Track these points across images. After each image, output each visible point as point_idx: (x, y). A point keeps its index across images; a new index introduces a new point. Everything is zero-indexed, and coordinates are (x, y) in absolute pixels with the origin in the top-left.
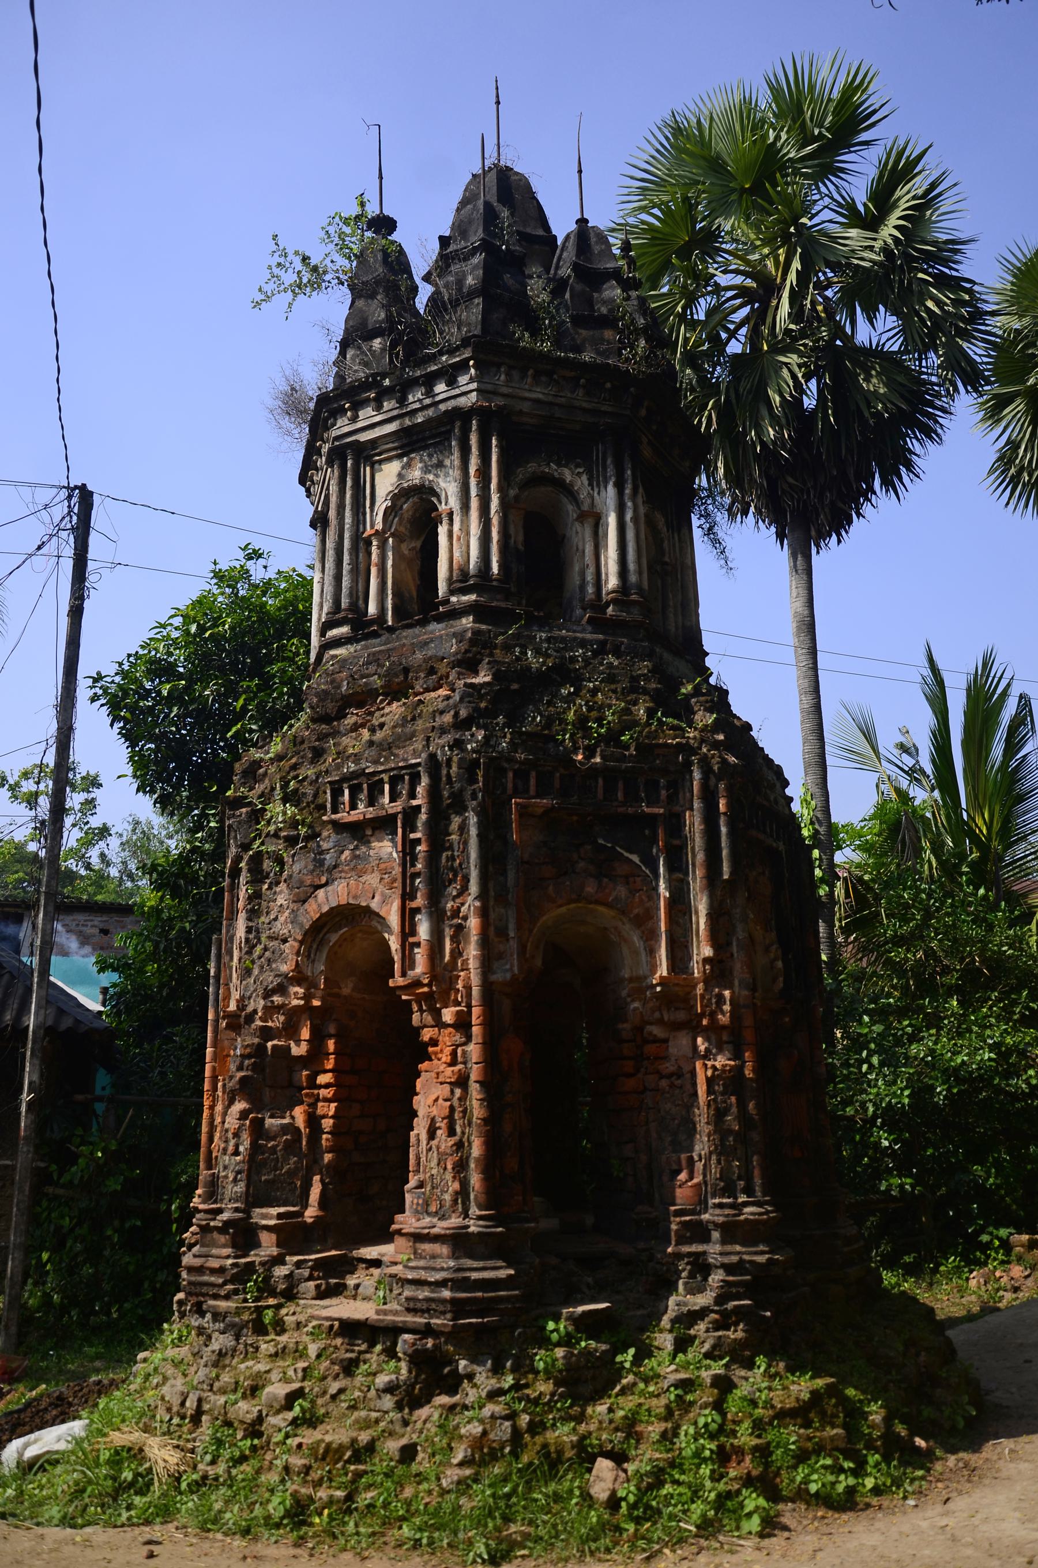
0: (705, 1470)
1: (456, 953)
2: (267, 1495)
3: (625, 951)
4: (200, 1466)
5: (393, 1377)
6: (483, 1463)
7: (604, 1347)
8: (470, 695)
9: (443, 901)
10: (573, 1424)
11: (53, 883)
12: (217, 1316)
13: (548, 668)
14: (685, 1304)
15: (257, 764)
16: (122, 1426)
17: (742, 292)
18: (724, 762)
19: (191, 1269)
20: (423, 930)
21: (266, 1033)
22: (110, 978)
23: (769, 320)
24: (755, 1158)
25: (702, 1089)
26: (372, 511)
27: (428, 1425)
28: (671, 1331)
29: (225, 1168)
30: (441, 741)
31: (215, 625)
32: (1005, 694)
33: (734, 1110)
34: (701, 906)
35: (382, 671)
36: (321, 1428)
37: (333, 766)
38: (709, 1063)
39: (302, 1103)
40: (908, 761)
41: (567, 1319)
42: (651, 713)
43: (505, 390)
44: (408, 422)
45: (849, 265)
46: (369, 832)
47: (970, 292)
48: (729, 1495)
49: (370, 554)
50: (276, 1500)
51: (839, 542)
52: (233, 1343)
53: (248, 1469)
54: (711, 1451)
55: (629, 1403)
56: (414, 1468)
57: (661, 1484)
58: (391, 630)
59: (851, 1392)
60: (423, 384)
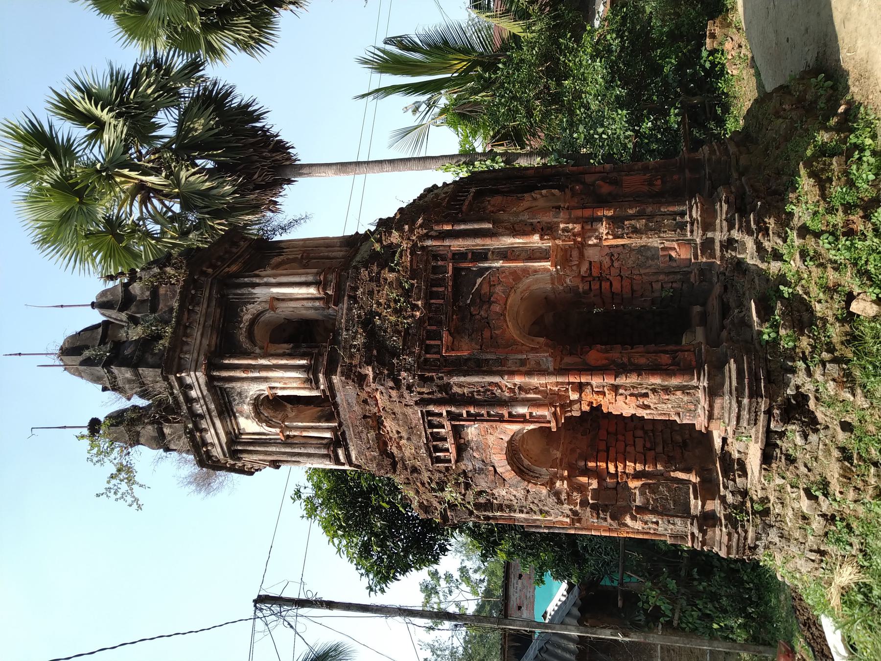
0: (859, 244)
1: (536, 390)
2: (873, 514)
4: (854, 553)
5: (797, 434)
7: (779, 304)
8: (380, 380)
11: (492, 620)
12: (758, 538)
13: (364, 332)
14: (752, 254)
15: (421, 505)
16: (827, 599)
17: (144, 202)
18: (421, 226)
19: (729, 553)
20: (522, 410)
21: (584, 503)
22: (548, 577)
23: (160, 188)
25: (620, 242)
26: (268, 435)
28: (769, 263)
29: (666, 530)
30: (408, 398)
32: (383, 51)
33: (633, 222)
34: (508, 241)
35: (365, 431)
36: (829, 479)
37: (423, 462)
38: (605, 237)
39: (626, 482)
40: (423, 107)
41: (761, 326)
42: (392, 270)
43: (195, 355)
44: (214, 413)
45: (126, 140)
46: (462, 441)
47: (142, 67)
49: (295, 436)
51: (293, 148)
52: (775, 529)
53: (855, 524)
54: (847, 240)
55: (814, 290)
56: (856, 423)
58: (340, 424)
59: (809, 153)
60: (191, 404)
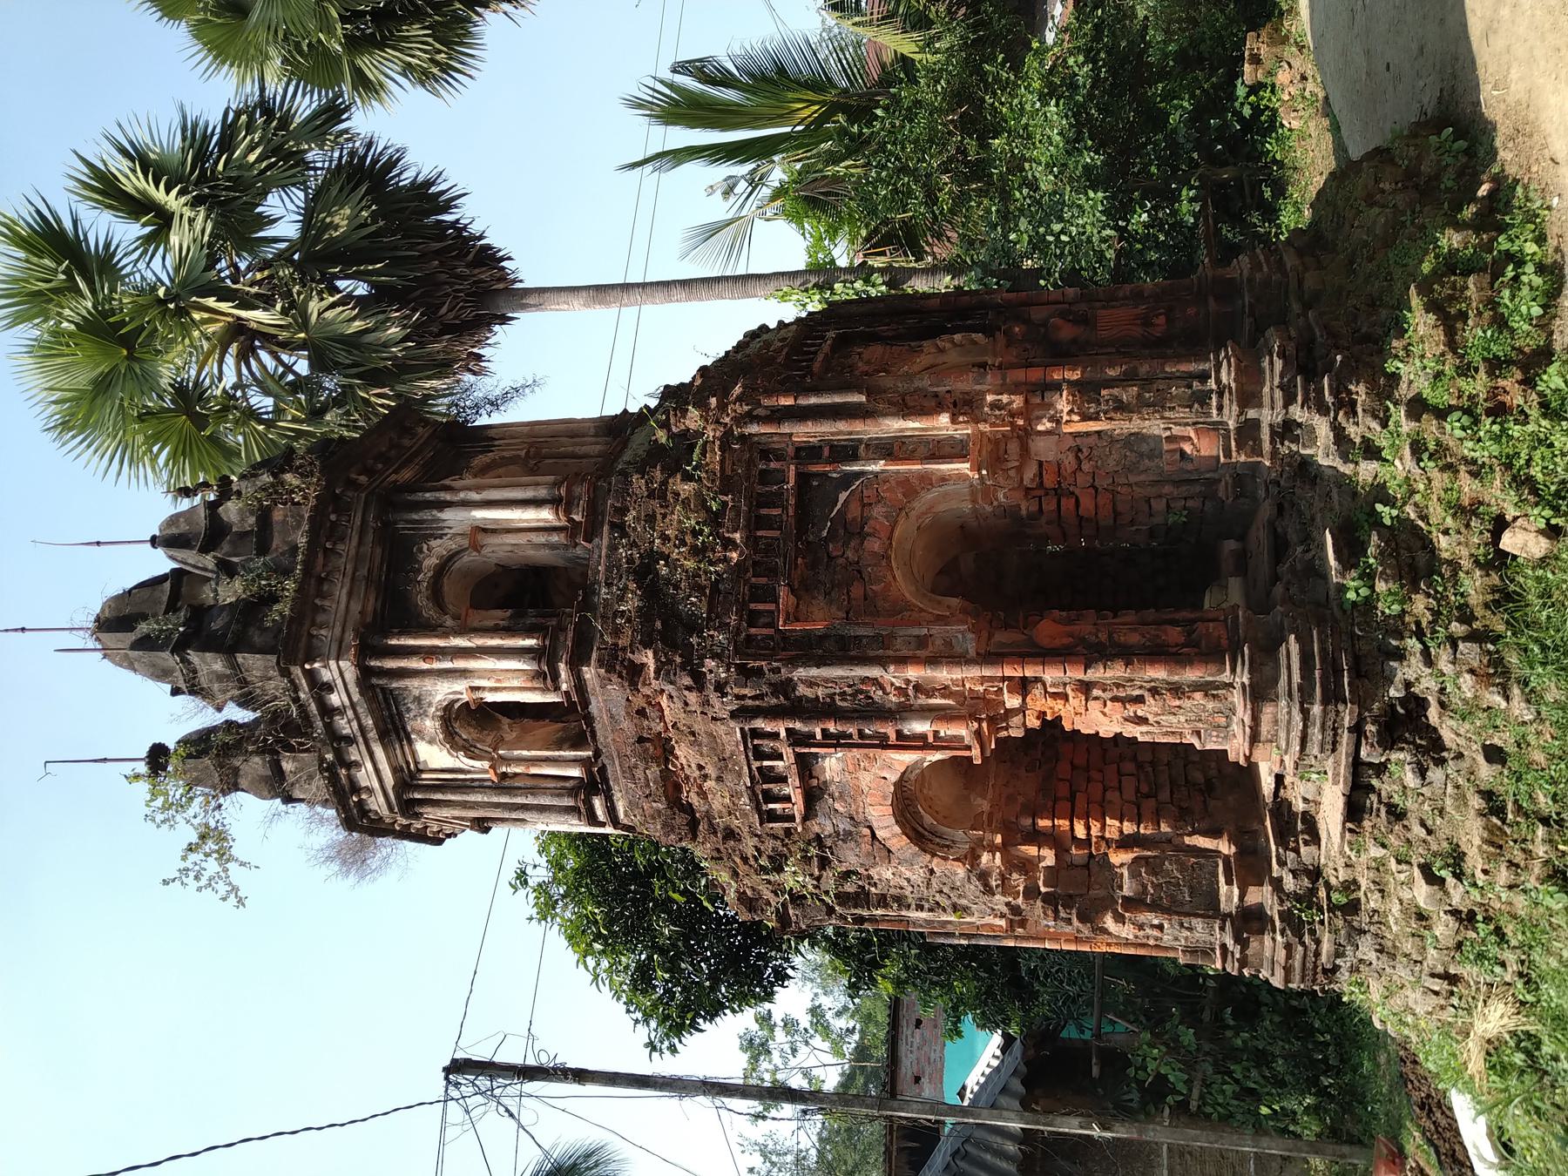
0: (1516, 431)
1: (945, 691)
2: (1541, 910)
3: (942, 508)
4: (1508, 979)
5: (1407, 767)
6: (1506, 673)
7: (1375, 538)
8: (668, 673)
9: (888, 705)
10: (1461, 574)
12: (1339, 953)
13: (639, 588)
14: (1327, 447)
15: (742, 897)
16: (1461, 1060)
17: (244, 356)
18: (739, 399)
19: (1287, 980)
20: (920, 727)
21: (1031, 893)
22: (968, 1023)
23: (272, 331)
24: (1168, 369)
25: (1093, 426)
26: (469, 772)
27: (1462, 731)
28: (1357, 463)
29: (1176, 939)
30: (717, 705)
31: (596, 922)
32: (671, 86)
33: (1115, 391)
35: (641, 765)
36: (1464, 848)
37: (745, 819)
38: (1065, 418)
41: (1344, 577)
42: (688, 478)
43: (338, 630)
44: (373, 735)
45: (210, 245)
46: (814, 782)
47: (238, 114)
48: (1544, 405)
49: (516, 775)
50: (1548, 901)
51: (509, 259)
52: (1368, 936)
54: (1494, 423)
55: (1437, 512)
56: (1511, 748)
57: (1530, 480)
